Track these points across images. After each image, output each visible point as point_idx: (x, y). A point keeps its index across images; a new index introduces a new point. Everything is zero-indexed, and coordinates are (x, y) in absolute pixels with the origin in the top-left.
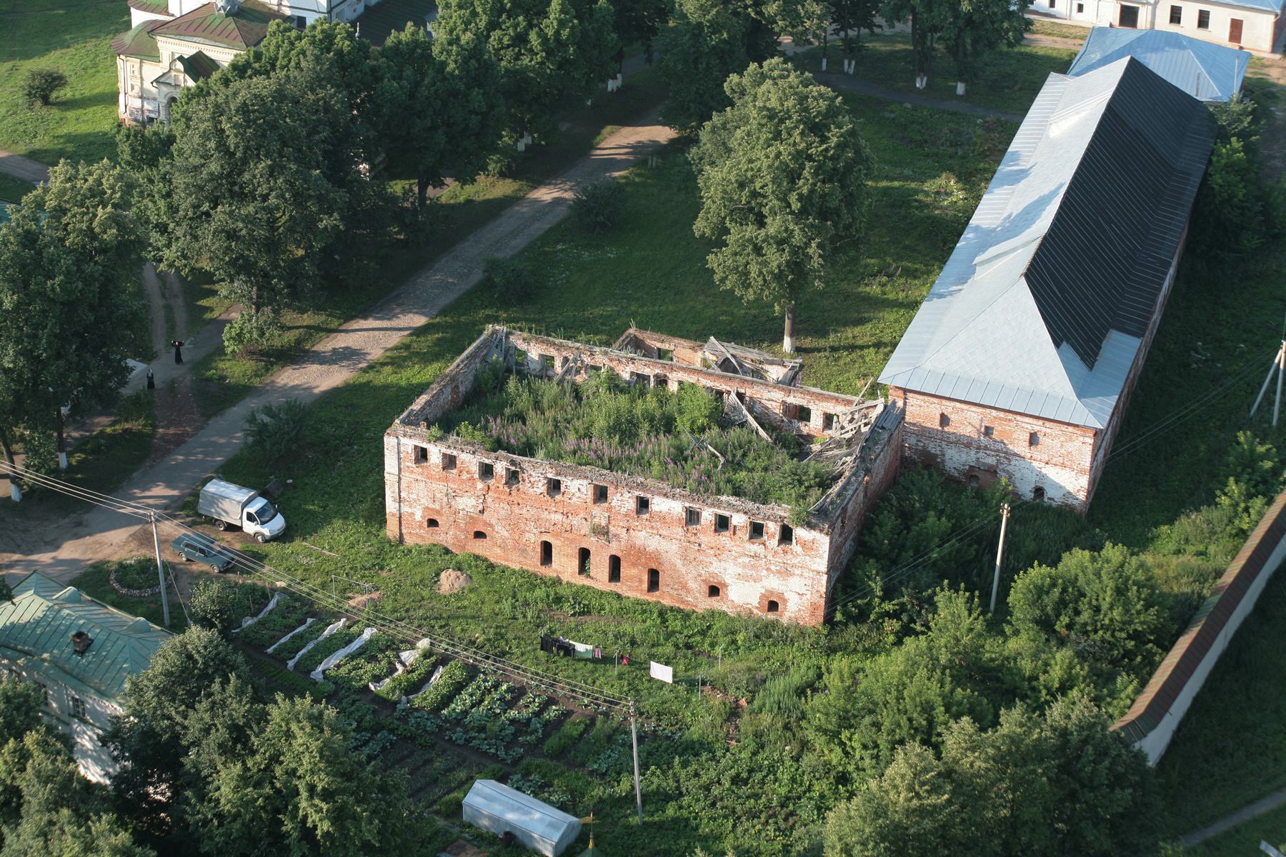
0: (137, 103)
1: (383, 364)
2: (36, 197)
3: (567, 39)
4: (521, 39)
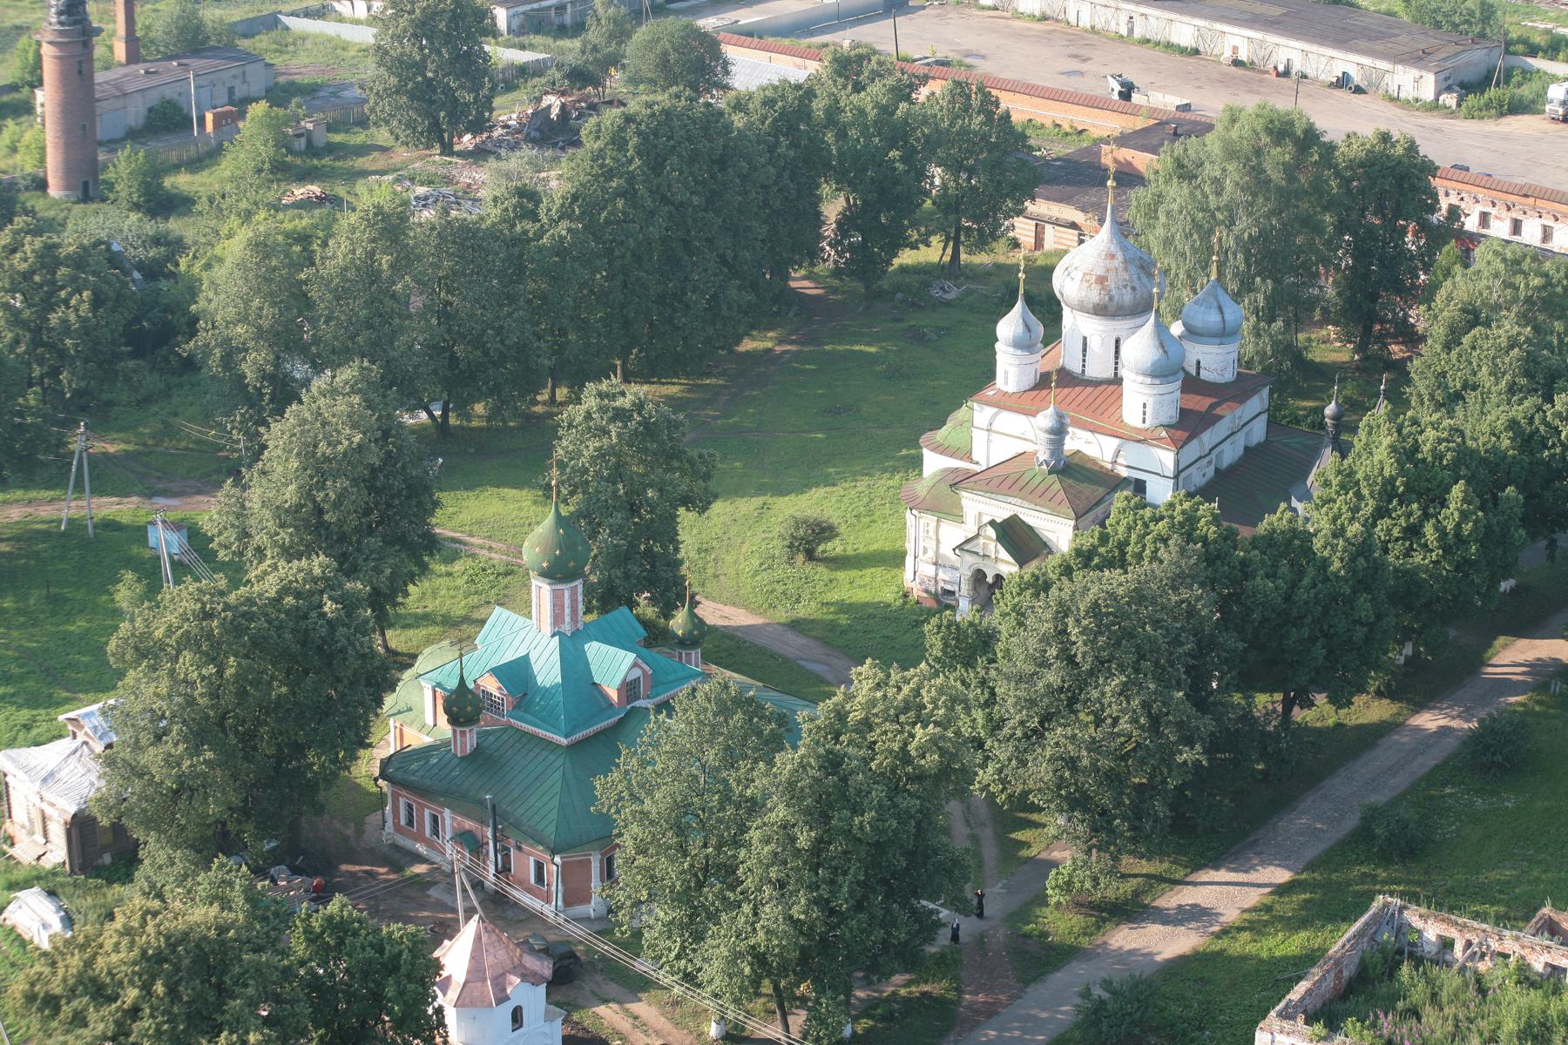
0: (929, 570)
1: (1240, 929)
2: (836, 705)
3: (1469, 535)
4: (1413, 532)
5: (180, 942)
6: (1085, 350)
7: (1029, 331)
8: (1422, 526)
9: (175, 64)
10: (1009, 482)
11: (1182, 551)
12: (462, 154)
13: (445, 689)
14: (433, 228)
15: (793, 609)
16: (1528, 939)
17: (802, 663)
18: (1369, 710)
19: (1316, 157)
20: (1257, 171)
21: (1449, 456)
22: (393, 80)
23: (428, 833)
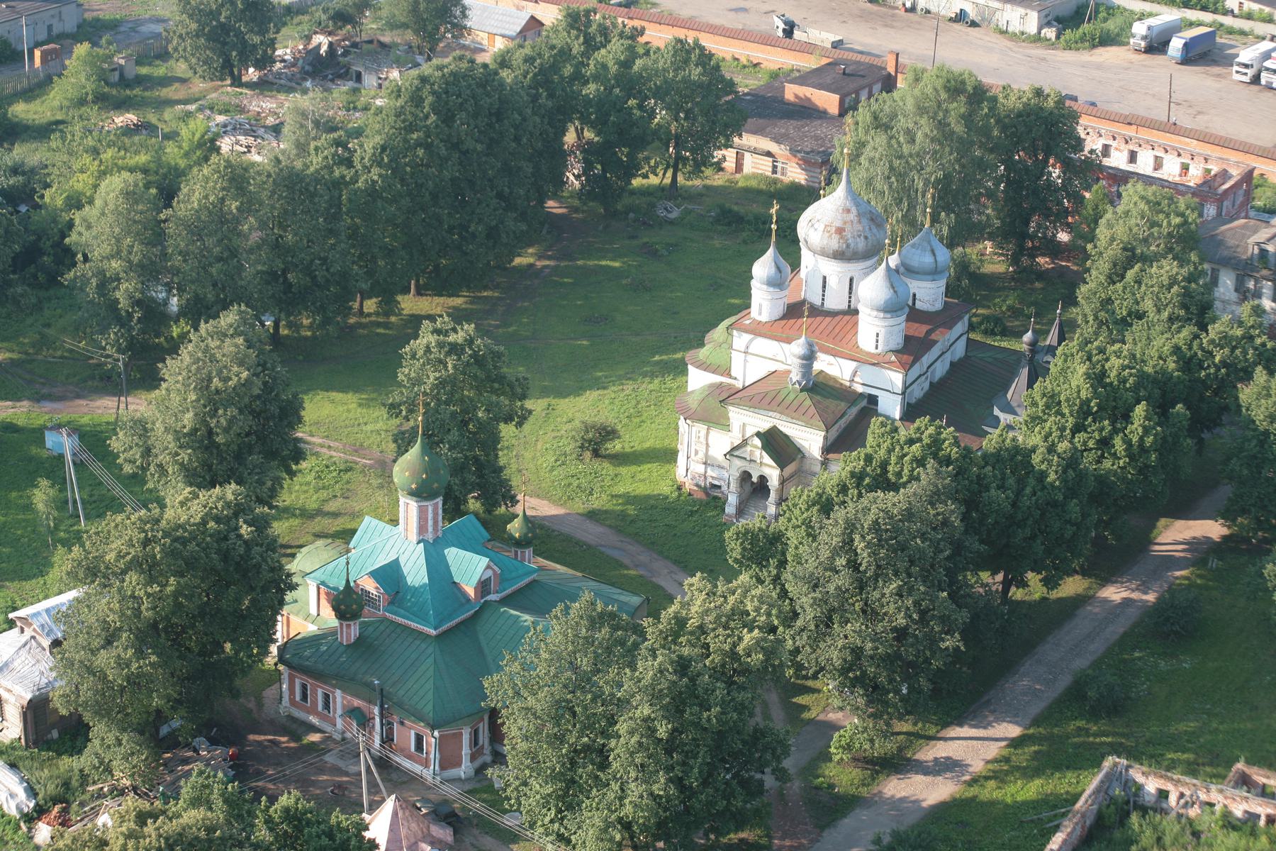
0: (700, 469)
1: (987, 778)
3: (1151, 446)
4: (1105, 443)
5: (176, 843)
6: (824, 287)
7: (780, 272)
8: (1112, 438)
9: (4, 6)
10: (768, 399)
11: (938, 473)
12: (250, 85)
13: (328, 587)
14: (269, 176)
15: (588, 500)
16: (1230, 791)
17: (603, 549)
18: (1072, 586)
19: (986, 110)
20: (942, 125)
21: (1131, 380)
22: (194, 26)
23: (320, 708)
